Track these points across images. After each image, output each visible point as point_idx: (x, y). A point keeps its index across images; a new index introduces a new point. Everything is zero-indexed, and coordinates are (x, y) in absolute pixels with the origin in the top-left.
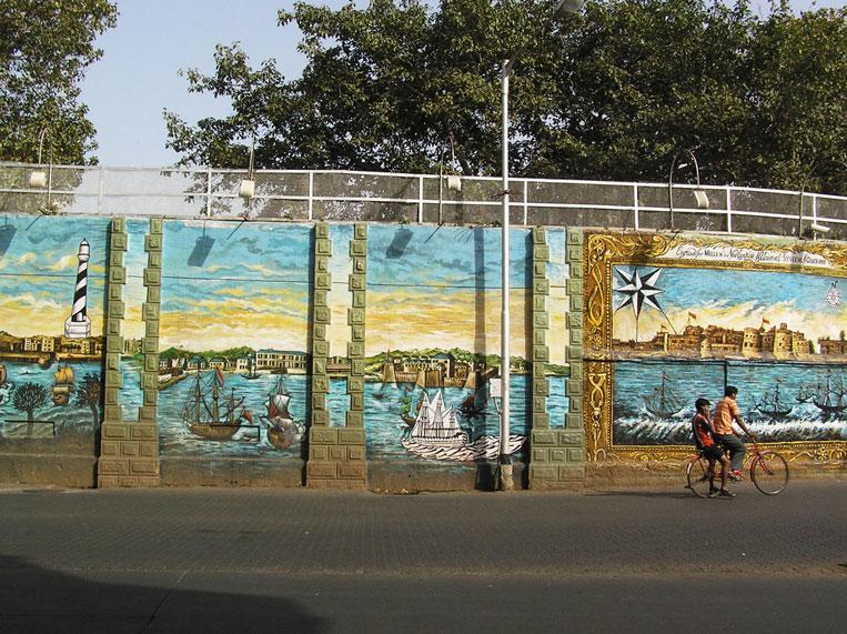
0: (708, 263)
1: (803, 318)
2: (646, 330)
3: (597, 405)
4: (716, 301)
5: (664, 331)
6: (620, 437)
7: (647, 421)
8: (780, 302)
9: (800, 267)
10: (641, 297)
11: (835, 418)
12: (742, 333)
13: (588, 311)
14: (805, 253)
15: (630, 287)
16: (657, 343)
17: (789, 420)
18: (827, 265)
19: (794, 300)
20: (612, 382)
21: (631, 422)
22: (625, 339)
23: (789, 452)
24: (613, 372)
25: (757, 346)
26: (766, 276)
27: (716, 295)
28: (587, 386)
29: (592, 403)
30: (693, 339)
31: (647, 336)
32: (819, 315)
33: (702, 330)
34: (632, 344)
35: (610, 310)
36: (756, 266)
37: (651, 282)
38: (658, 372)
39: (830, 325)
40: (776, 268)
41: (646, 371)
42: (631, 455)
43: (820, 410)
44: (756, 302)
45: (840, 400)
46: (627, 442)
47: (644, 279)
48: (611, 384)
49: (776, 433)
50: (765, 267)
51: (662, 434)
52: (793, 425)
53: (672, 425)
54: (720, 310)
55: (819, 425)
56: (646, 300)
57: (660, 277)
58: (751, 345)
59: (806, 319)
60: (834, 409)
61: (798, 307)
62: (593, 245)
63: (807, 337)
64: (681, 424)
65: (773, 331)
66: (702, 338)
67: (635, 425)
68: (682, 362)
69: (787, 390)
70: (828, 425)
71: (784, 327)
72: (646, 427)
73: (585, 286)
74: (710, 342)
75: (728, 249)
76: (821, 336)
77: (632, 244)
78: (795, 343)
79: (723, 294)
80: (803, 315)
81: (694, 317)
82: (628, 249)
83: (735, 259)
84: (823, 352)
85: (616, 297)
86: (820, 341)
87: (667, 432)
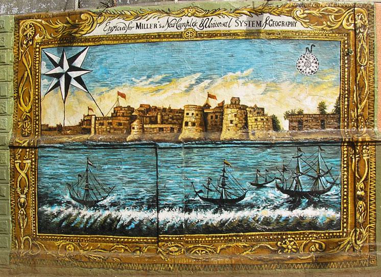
0: (140, 37)
1: (261, 90)
2: (74, 113)
3: (22, 192)
4: (149, 77)
5: (91, 113)
6: (45, 225)
7: (71, 210)
8: (230, 74)
9: (259, 32)
10: (68, 79)
11: (308, 205)
12: (182, 112)
13: (18, 97)
14: (266, 15)
15: (58, 70)
16: (84, 127)
17: (241, 208)
18: (299, 27)
19: (251, 69)
20: (37, 169)
21: (55, 209)
22: (53, 124)
23: (240, 244)
24: (37, 159)
25: (200, 125)
26: (213, 45)
27: (149, 71)
28: (14, 173)
29: (19, 190)
30: (123, 120)
31: (73, 120)
32: (286, 87)
33: (132, 110)
34: (60, 129)
35: (39, 95)
36: (199, 35)
37: (78, 63)
38: (81, 158)
39: (301, 97)
40: (225, 35)
41: (69, 156)
42: (57, 243)
43: (286, 196)
44: (198, 75)
45: (315, 184)
46: (52, 231)
47: (71, 61)
48: (35, 170)
49: (222, 224)
50: (211, 35)
51: (87, 222)
52: (247, 213)
53: (97, 214)
54: (153, 86)
55: (284, 213)
56: (74, 83)
57: (86, 57)
58: (194, 124)
59: (266, 91)
60: (306, 195)
61: (255, 79)
62: (24, 31)
63: (269, 112)
64: (107, 213)
65: (221, 107)
66: (133, 119)
67: (59, 213)
68: (106, 147)
69: (237, 174)
70: (298, 213)
71: (235, 102)
72: (70, 215)
73: (16, 72)
74: (142, 123)
75: (164, 20)
76: (289, 110)
77: (60, 25)
78: (251, 120)
79: (157, 70)
80: (263, 86)
81: (123, 96)
82: (57, 31)
83: (173, 30)
84: (291, 128)
85: (44, 82)
86: (288, 116)
87: (92, 221)
